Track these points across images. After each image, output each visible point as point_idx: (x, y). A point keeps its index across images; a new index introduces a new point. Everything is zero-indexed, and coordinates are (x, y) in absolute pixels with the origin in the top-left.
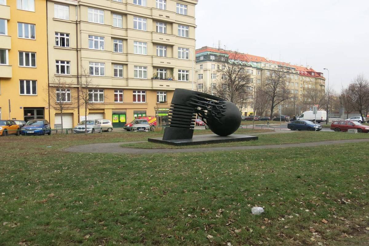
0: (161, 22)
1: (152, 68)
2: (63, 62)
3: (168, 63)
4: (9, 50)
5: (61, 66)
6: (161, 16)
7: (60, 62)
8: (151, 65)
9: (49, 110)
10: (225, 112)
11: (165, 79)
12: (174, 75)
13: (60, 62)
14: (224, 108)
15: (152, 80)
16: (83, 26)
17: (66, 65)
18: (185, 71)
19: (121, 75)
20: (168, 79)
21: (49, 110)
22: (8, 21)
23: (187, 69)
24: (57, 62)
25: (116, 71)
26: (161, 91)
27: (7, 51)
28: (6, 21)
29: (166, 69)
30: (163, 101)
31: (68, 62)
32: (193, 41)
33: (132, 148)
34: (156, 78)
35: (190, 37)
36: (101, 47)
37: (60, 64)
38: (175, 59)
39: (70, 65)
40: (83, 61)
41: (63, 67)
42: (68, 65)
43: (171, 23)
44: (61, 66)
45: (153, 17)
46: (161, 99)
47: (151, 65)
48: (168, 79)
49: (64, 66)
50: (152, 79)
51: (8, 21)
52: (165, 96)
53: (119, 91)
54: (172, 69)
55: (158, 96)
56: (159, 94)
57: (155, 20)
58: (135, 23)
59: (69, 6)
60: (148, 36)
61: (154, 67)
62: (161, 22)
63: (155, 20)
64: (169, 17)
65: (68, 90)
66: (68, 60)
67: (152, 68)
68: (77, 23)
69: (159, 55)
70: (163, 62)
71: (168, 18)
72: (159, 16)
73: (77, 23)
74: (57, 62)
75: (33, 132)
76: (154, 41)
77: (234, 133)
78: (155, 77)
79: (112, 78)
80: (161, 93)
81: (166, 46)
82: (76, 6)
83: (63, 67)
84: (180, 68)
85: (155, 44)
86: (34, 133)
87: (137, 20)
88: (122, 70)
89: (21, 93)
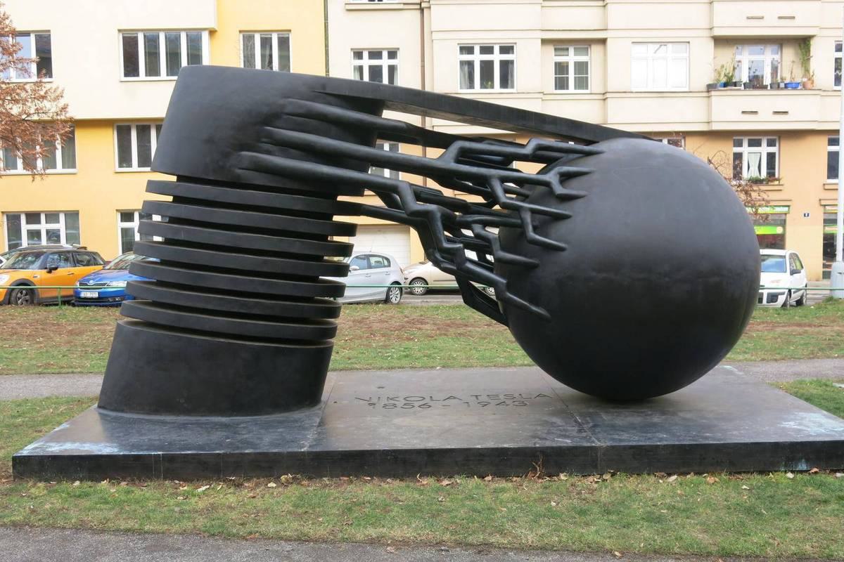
1: (712, 43)
2: (375, 54)
3: (752, 18)
4: (212, 32)
5: (371, 67)
7: (366, 55)
8: (707, 33)
10: (562, 227)
11: (775, 86)
12: (814, 64)
13: (366, 55)
14: (559, 190)
15: (708, 92)
17: (497, 57)
18: (385, 54)
19: (582, 83)
20: (782, 85)
23: (506, 39)
24: (358, 55)
25: (561, 68)
26: (755, 138)
27: (205, 36)
29: (780, 42)
30: (764, 174)
31: (393, 54)
33: (68, 373)
34: (725, 85)
37: (477, 58)
40: (436, 45)
41: (487, 67)
42: (392, 62)
44: (371, 67)
46: (754, 168)
47: (707, 33)
48: (782, 85)
49: (575, 63)
50: (710, 88)
52: (771, 157)
53: (750, 141)
54: (803, 43)
55: (738, 157)
56: (745, 149)
65: (771, 143)
66: (392, 45)
70: (762, 18)
74: (358, 55)
75: (96, 295)
78: (724, 80)
79: (541, 95)
80: (755, 143)
83: (487, 67)
84: (468, 39)
86: (99, 298)
88: (587, 63)
89: (121, 166)
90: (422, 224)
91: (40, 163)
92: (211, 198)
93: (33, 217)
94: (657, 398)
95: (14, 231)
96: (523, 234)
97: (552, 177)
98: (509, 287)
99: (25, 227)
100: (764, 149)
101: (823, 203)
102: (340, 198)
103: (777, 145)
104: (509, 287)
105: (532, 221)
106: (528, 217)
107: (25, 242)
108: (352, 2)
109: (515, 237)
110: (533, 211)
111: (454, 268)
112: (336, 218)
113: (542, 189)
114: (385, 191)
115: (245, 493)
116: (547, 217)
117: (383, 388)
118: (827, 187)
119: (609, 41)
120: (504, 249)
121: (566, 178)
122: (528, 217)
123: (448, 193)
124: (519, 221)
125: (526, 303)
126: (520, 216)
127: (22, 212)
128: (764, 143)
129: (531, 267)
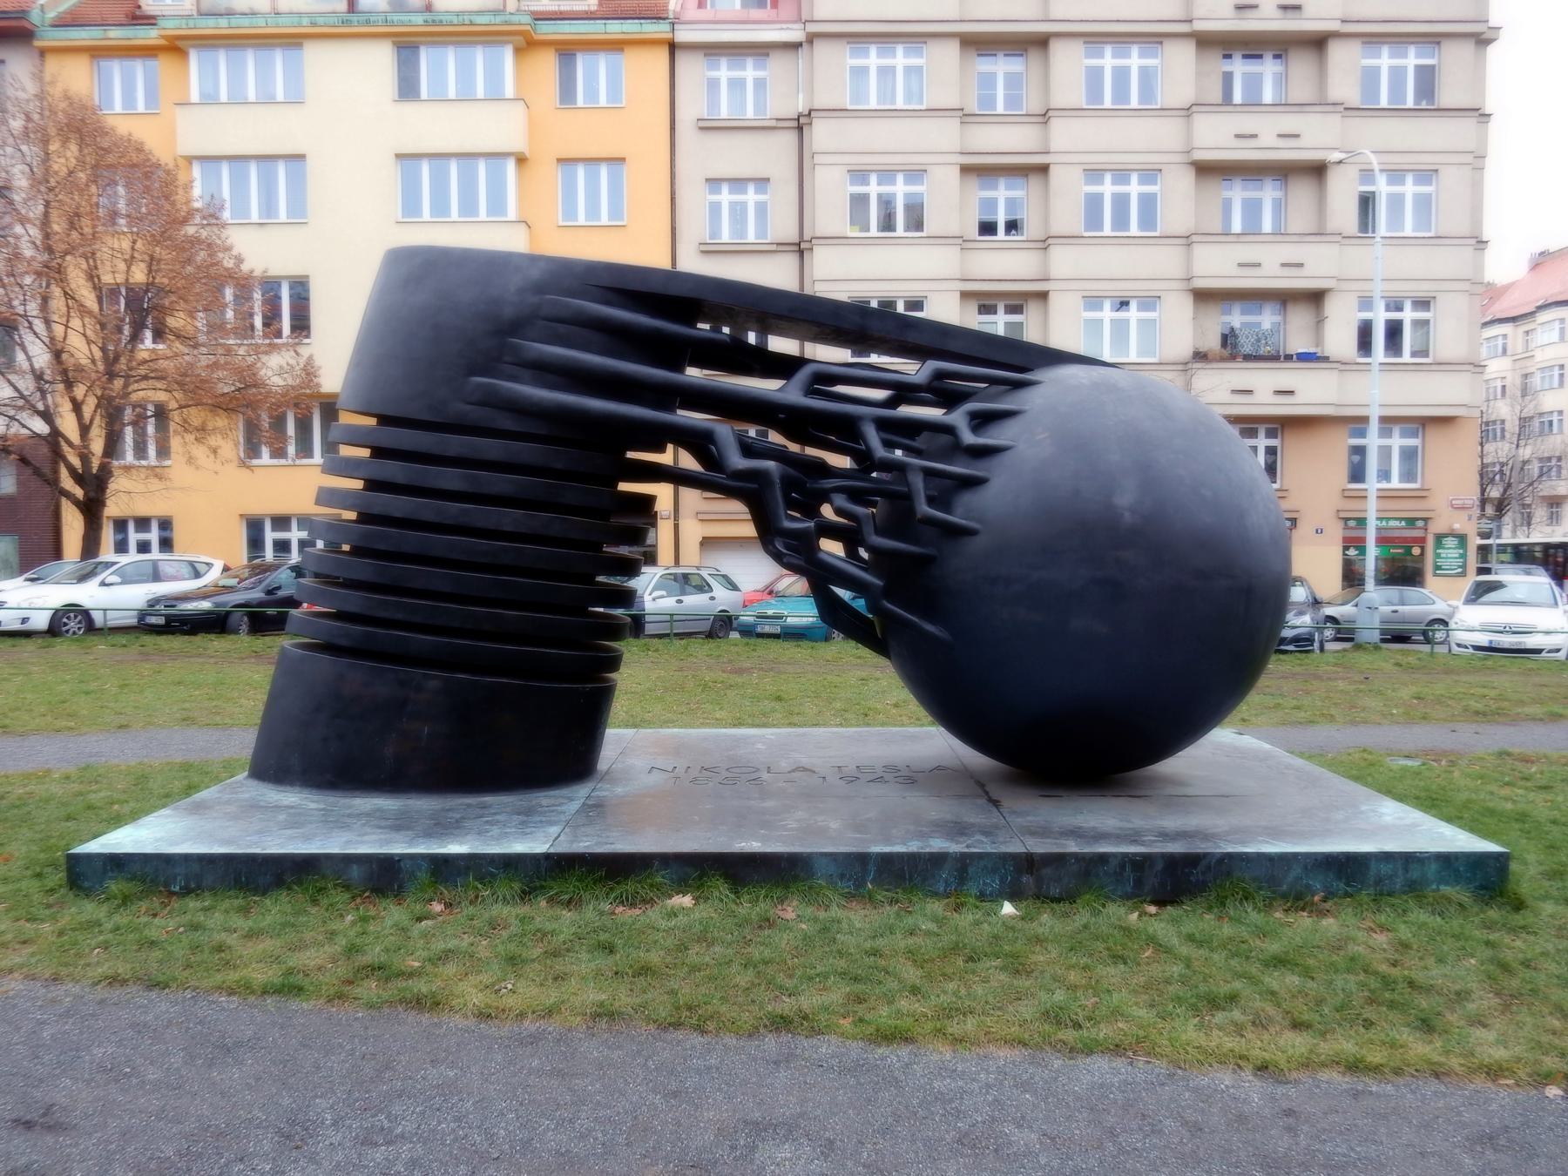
0: (1252, 46)
6: (1249, 13)
7: (1408, 305)
9: (676, 527)
14: (969, 438)
16: (822, 134)
17: (1408, 315)
21: (676, 527)
22: (521, 160)
28: (511, 165)
29: (1284, 298)
32: (1468, 124)
35: (1448, 95)
36: (28, 226)
38: (1338, 238)
39: (1435, 317)
43: (1318, 43)
45: (1199, 26)
51: (521, 160)
52: (1271, 451)
54: (1316, 298)
57: (1208, 42)
58: (1095, 76)
59: (1439, 43)
60: (1160, 136)
61: (1204, 297)
62: (1252, 46)
63: (1208, 42)
64: (1297, 8)
67: (1187, 303)
68: (800, 125)
69: (1237, 226)
71: (1290, 14)
72: (1279, 14)
73: (800, 125)
76: (1200, 156)
77: (1245, 707)
79: (1470, 368)
81: (1283, 172)
82: (796, 46)
85: (1207, 170)
87: (1108, 60)
90: (749, 490)
91: (291, 450)
92: (436, 450)
93: (281, 522)
94: (1172, 766)
95: (256, 543)
96: (910, 510)
97: (958, 418)
98: (888, 593)
99: (270, 536)
100: (1262, 442)
101: (1343, 515)
102: (630, 455)
103: (1279, 436)
104: (888, 593)
105: (926, 488)
106: (918, 482)
107: (269, 554)
108: (566, 7)
109: (901, 519)
110: (929, 473)
111: (802, 563)
112: (624, 487)
113: (944, 439)
114: (698, 442)
115: (589, 913)
116: (948, 482)
117: (121, 727)
118: (1347, 494)
119: (1053, 170)
120: (880, 532)
121: (982, 420)
122: (918, 482)
123: (794, 448)
124: (906, 489)
125: (889, 606)
126: (906, 481)
127: (267, 515)
128: (1262, 434)
129: (925, 562)
